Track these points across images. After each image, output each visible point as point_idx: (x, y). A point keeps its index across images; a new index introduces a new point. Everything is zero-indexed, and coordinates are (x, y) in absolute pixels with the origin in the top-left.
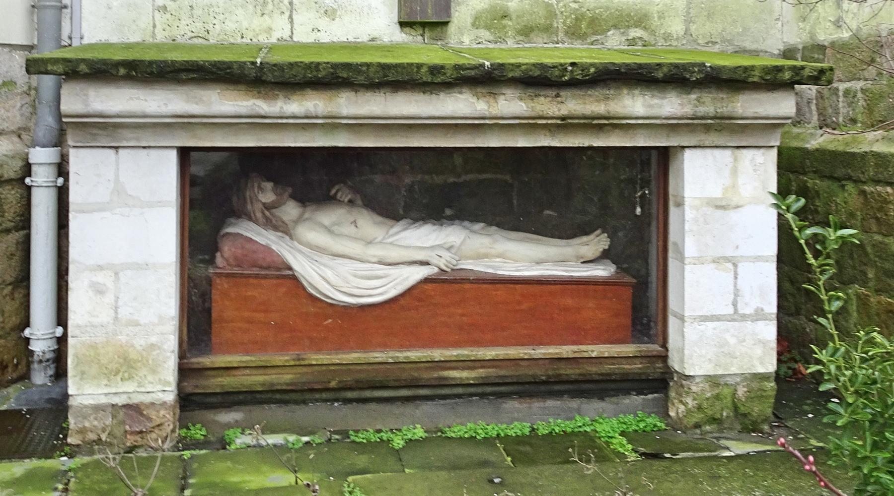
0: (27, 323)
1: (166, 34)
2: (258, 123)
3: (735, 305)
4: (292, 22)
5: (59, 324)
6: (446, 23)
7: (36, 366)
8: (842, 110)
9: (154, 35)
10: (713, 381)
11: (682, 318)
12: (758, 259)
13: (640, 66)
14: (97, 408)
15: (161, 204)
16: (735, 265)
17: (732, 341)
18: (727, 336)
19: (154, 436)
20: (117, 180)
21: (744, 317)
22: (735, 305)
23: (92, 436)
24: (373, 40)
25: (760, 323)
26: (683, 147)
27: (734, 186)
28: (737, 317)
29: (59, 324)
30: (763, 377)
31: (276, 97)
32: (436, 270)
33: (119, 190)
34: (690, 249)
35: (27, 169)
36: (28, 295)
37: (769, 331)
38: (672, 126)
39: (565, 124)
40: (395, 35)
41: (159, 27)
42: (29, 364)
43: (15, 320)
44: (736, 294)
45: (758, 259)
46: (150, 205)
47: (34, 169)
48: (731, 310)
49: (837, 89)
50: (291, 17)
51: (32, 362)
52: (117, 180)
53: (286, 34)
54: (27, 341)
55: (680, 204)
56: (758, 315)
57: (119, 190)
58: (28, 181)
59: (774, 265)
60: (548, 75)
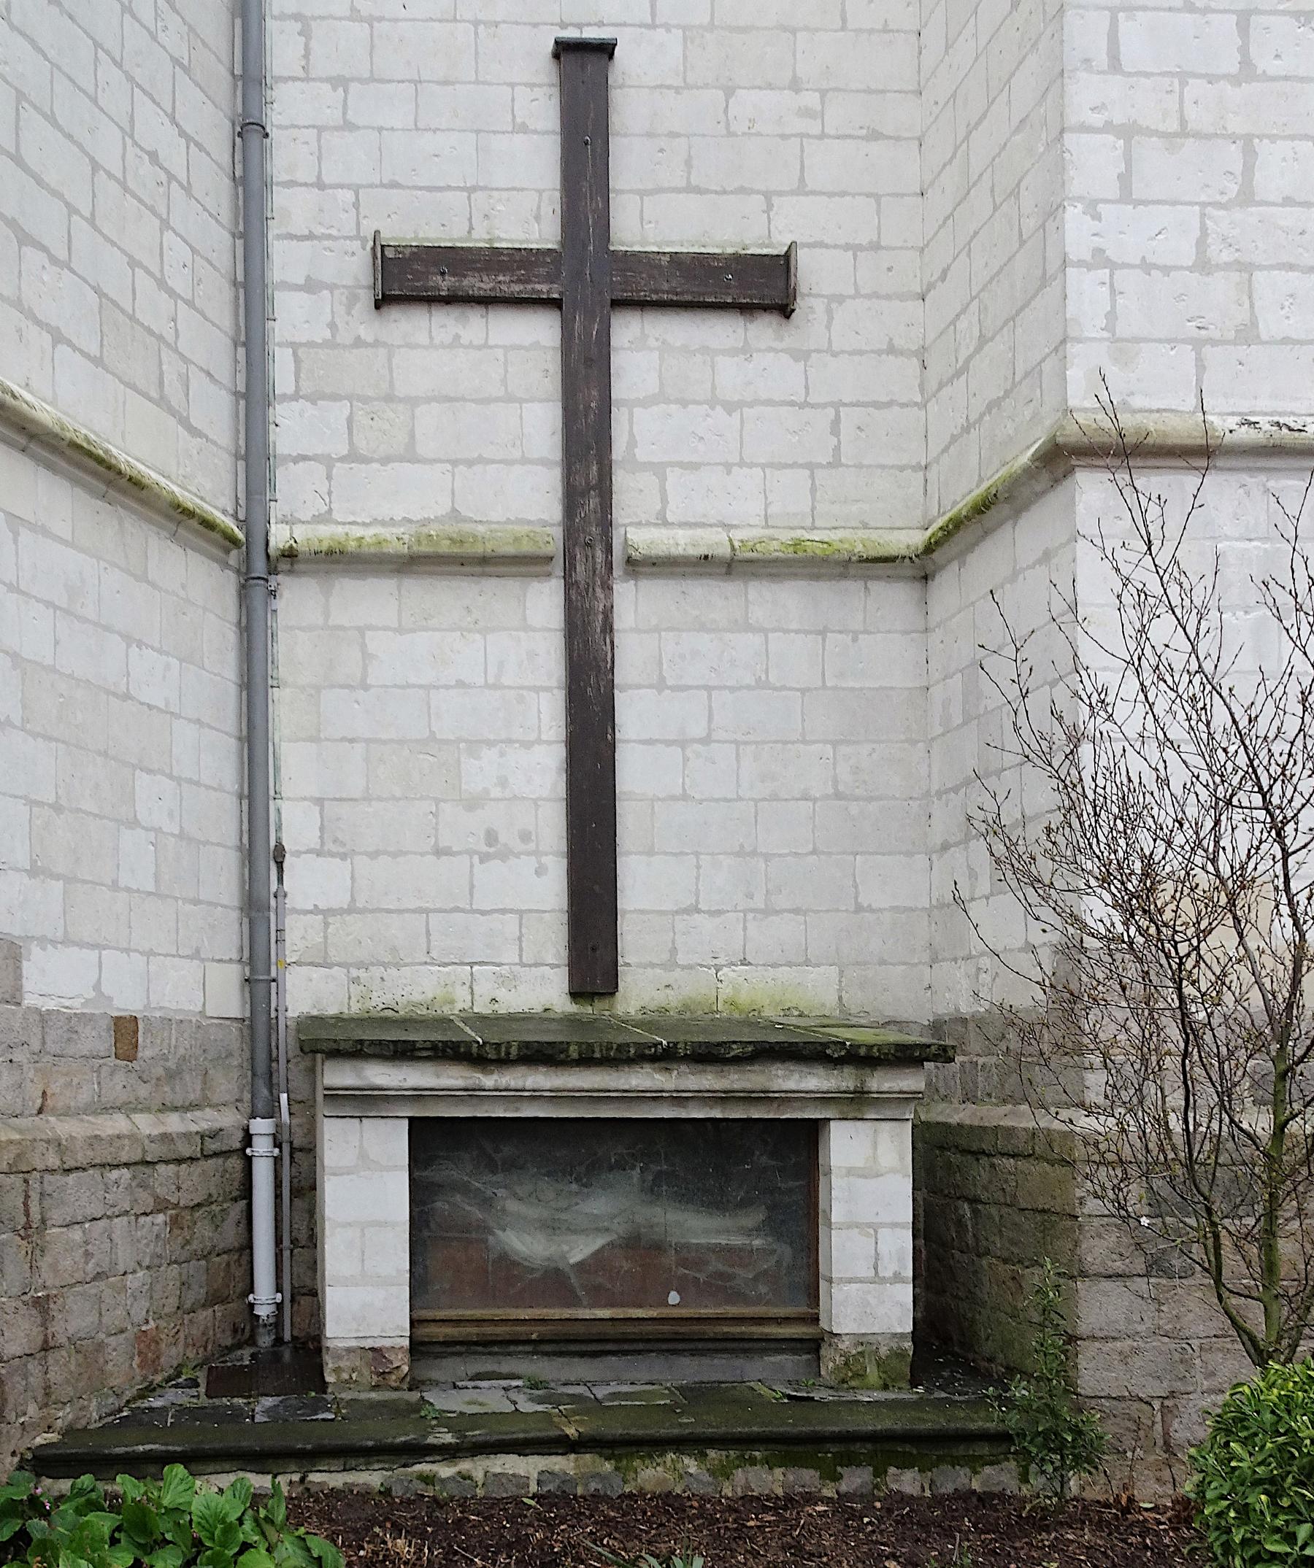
0: (252, 1291)
1: (359, 1005)
2: (472, 1094)
3: (876, 1269)
4: (472, 993)
5: (278, 1291)
6: (612, 994)
7: (261, 1330)
8: (981, 1085)
9: (349, 1008)
10: (860, 1339)
11: (830, 1281)
12: (895, 1225)
13: (791, 1044)
14: (349, 1350)
15: (395, 1168)
16: (876, 1232)
17: (873, 1301)
18: (870, 1298)
19: (394, 1377)
20: (361, 1146)
21: (883, 1280)
22: (876, 1269)
23: (345, 1376)
24: (546, 1010)
25: (898, 1285)
26: (829, 1120)
27: (875, 1158)
28: (877, 1279)
29: (278, 1291)
30: (902, 1335)
31: (492, 1073)
32: (615, 1236)
33: (363, 1156)
34: (835, 1217)
35: (248, 1139)
36: (251, 1262)
37: (905, 1293)
38: (824, 1099)
39: (726, 1098)
40: (569, 1007)
41: (354, 999)
42: (253, 1330)
43: (240, 1287)
44: (877, 1259)
45: (895, 1225)
46: (388, 1169)
47: (255, 1140)
48: (872, 1273)
49: (976, 1063)
50: (471, 988)
51: (258, 1326)
52: (361, 1146)
53: (467, 1005)
54: (252, 1306)
55: (828, 1173)
56: (897, 1278)
57: (363, 1156)
58: (248, 1151)
59: (909, 1234)
60: (385, 550)
